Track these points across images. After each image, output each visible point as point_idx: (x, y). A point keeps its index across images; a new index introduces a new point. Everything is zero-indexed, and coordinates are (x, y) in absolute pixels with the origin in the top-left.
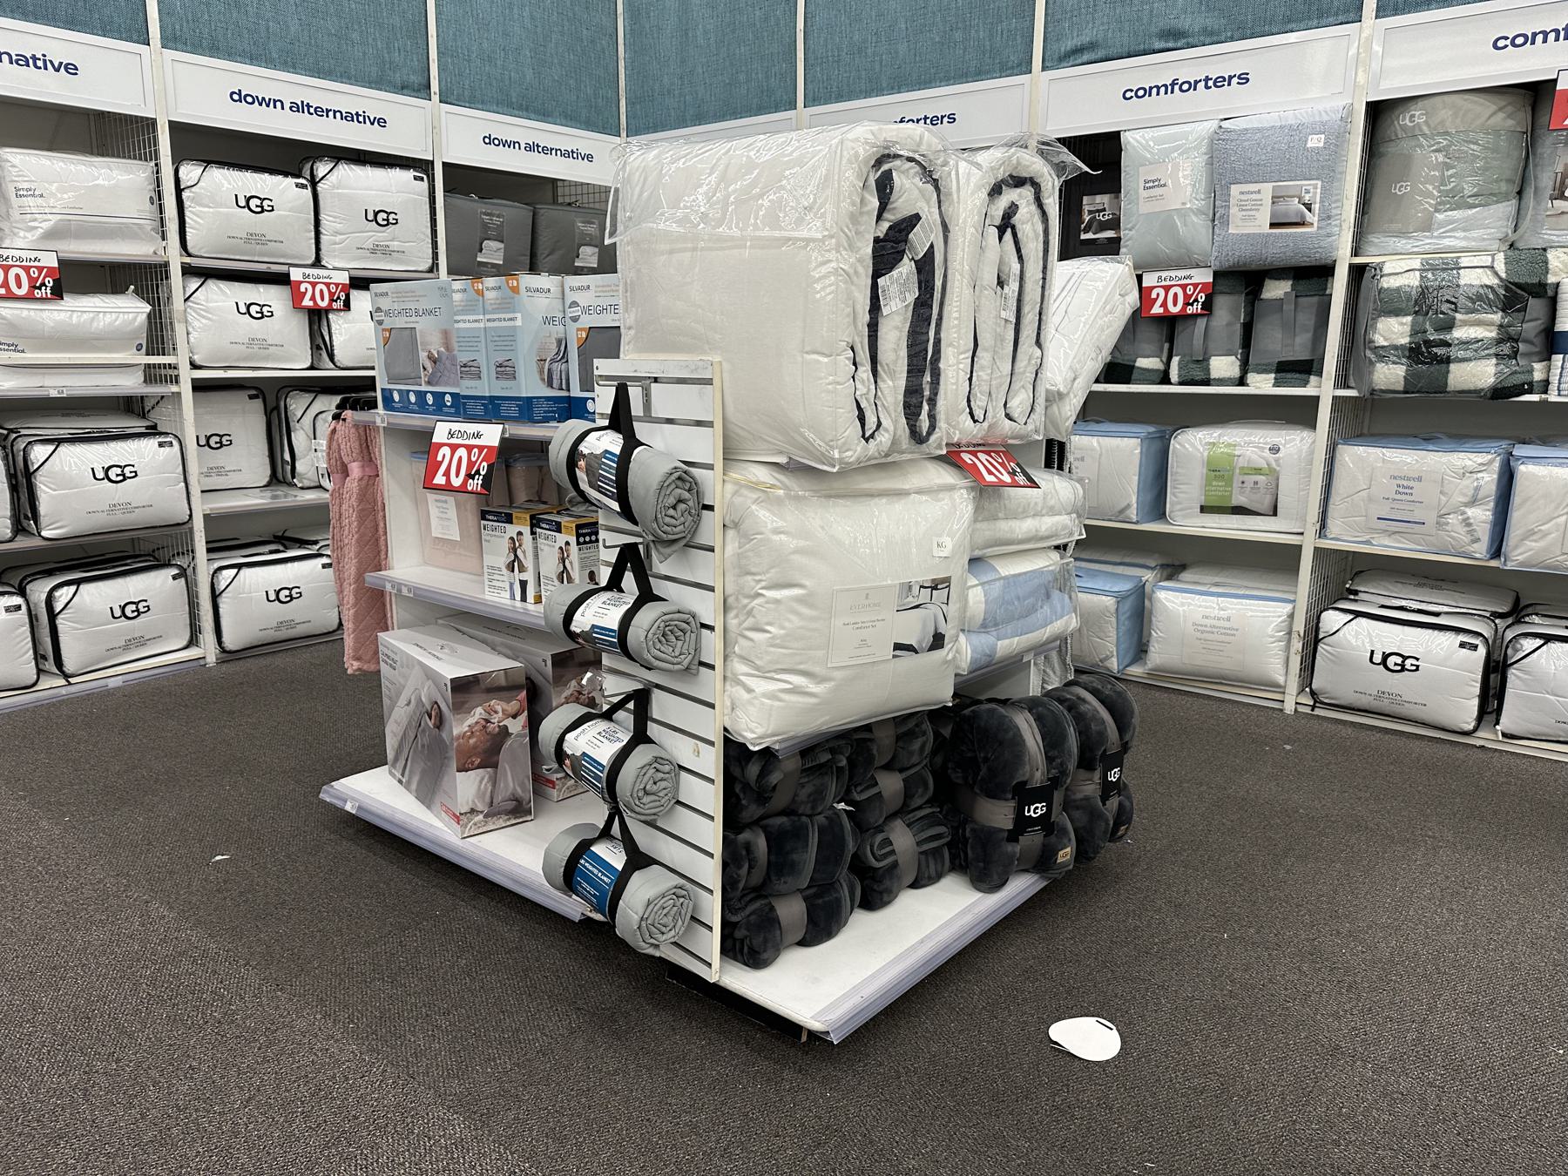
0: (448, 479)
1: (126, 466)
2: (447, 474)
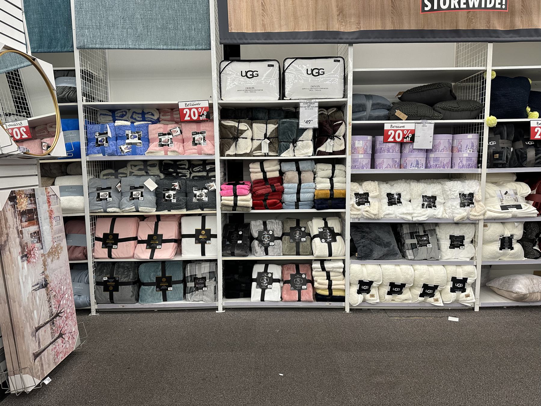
1: (320, 69)
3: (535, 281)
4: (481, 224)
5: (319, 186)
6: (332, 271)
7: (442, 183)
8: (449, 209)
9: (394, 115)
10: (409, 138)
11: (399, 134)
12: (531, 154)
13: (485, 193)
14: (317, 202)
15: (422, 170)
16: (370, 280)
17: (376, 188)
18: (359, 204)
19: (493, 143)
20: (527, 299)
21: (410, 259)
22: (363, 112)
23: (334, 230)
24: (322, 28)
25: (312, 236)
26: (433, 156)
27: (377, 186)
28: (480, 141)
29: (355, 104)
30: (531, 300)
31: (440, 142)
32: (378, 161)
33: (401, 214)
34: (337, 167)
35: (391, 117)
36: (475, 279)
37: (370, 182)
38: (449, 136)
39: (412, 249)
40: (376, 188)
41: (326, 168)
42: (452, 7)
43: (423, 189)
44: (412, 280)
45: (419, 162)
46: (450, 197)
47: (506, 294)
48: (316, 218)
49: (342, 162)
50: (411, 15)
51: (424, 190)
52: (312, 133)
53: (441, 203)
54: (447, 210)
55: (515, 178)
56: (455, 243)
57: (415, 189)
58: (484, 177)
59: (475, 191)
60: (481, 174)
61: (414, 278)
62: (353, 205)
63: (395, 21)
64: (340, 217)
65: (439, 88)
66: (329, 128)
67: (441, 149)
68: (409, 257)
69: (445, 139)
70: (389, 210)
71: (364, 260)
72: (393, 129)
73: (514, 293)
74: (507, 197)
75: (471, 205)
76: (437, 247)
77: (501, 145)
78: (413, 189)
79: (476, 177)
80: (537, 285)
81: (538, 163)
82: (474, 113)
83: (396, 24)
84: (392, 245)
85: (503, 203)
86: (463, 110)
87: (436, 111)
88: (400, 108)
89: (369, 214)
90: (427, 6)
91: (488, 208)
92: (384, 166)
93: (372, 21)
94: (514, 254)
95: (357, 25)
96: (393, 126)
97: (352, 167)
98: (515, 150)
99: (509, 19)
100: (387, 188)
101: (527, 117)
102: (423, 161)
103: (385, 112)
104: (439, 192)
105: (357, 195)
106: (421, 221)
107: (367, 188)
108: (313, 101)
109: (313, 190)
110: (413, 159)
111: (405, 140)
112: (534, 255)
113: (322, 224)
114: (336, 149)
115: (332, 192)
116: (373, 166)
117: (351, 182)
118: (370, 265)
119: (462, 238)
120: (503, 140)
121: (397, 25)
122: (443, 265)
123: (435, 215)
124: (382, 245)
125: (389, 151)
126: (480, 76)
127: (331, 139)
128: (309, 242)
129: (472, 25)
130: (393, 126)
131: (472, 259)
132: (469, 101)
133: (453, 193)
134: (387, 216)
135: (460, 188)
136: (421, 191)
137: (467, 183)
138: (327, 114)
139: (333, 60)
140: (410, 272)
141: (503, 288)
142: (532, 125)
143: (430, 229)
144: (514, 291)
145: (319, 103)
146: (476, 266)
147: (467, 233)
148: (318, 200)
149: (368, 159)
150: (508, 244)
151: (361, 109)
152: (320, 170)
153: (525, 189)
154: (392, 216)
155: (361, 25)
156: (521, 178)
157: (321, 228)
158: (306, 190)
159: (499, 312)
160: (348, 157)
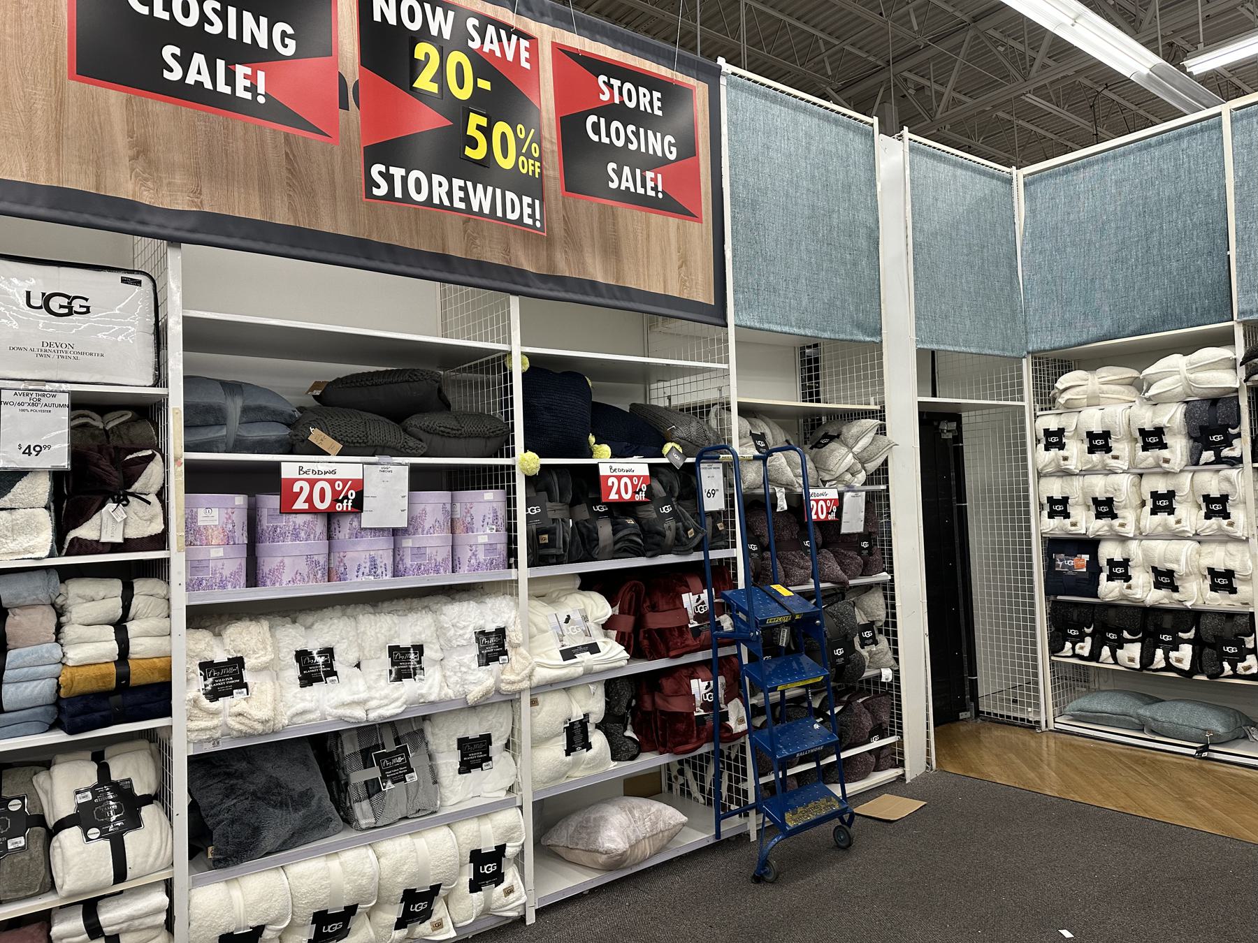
0: (818, 516)
2: (817, 513)
3: (637, 813)
4: (526, 700)
5: (76, 655)
6: (127, 931)
7: (435, 607)
8: (455, 673)
9: (305, 440)
10: (350, 501)
11: (322, 491)
12: (605, 530)
13: (528, 623)
14: (70, 709)
15: (385, 582)
16: (254, 924)
17: (263, 642)
18: (214, 695)
19: (536, 510)
20: (628, 861)
21: (364, 827)
22: (218, 427)
23: (131, 789)
24: (80, 181)
25: (51, 822)
26: (410, 545)
27: (268, 635)
28: (509, 506)
29: (192, 405)
30: (634, 860)
31: (424, 510)
32: (267, 564)
33: (336, 707)
34: (141, 586)
35: (298, 445)
36: (521, 842)
37: (248, 623)
38: (443, 496)
39: (369, 797)
40: (263, 642)
41: (102, 594)
42: (436, 201)
43: (390, 630)
44: (373, 888)
45: (378, 562)
46: (455, 643)
47: (584, 858)
48: (69, 757)
49: (158, 570)
50: (338, 199)
51: (392, 632)
52: (49, 483)
53: (434, 662)
54: (450, 677)
55: (578, 582)
56: (472, 756)
57: (371, 632)
58: (523, 587)
59: (507, 622)
60: (517, 581)
61: (380, 879)
62: (195, 702)
63: (298, 207)
64: (158, 744)
65: (414, 381)
66: (111, 469)
67: (427, 527)
68: (364, 823)
69: (434, 501)
70: (303, 700)
71: (236, 864)
72: (305, 476)
73: (601, 853)
74: (570, 628)
75: (501, 658)
76: (429, 776)
77: (551, 515)
78: (364, 633)
79: (508, 588)
80: (642, 822)
81: (619, 549)
82: (493, 444)
83: (300, 214)
84: (316, 798)
85: (564, 643)
86: (470, 436)
87: (410, 435)
88: (322, 423)
89: (247, 721)
90: (378, 187)
91: (538, 659)
92: (286, 577)
93: (236, 194)
94: (593, 759)
95: (191, 195)
96: (304, 470)
97: (191, 586)
98: (576, 523)
99: (545, 253)
100: (295, 637)
101: (590, 456)
102: (386, 559)
103: (278, 432)
104: (429, 632)
105: (207, 667)
106: (388, 718)
107: (238, 642)
108: (48, 387)
109: (56, 669)
110: (363, 555)
111: (339, 507)
112: (628, 750)
113: (87, 774)
114: (133, 533)
115: (124, 670)
116: (253, 578)
117: (187, 628)
118: (253, 877)
119: (486, 740)
120: (553, 504)
121: (304, 218)
122: (449, 825)
123: (422, 696)
124: (287, 806)
125: (296, 536)
126: (499, 362)
127: (118, 502)
128: (37, 849)
129: (475, 250)
130: (304, 470)
131: (510, 790)
132: (480, 416)
133: (461, 632)
134: (299, 720)
135: (477, 619)
136: (385, 636)
137: (490, 605)
138: (101, 427)
139: (119, 276)
140: (368, 865)
141: (577, 844)
142: (602, 473)
143: (411, 730)
144: (601, 850)
145: (73, 395)
146: (521, 807)
147: (496, 725)
148: (71, 700)
149: (239, 560)
150: (581, 736)
151: (212, 420)
152: (80, 600)
153: (599, 607)
154: (311, 716)
155: (205, 197)
156: (589, 583)
157: (86, 790)
158: (26, 669)
159: (574, 910)
160: (176, 556)
